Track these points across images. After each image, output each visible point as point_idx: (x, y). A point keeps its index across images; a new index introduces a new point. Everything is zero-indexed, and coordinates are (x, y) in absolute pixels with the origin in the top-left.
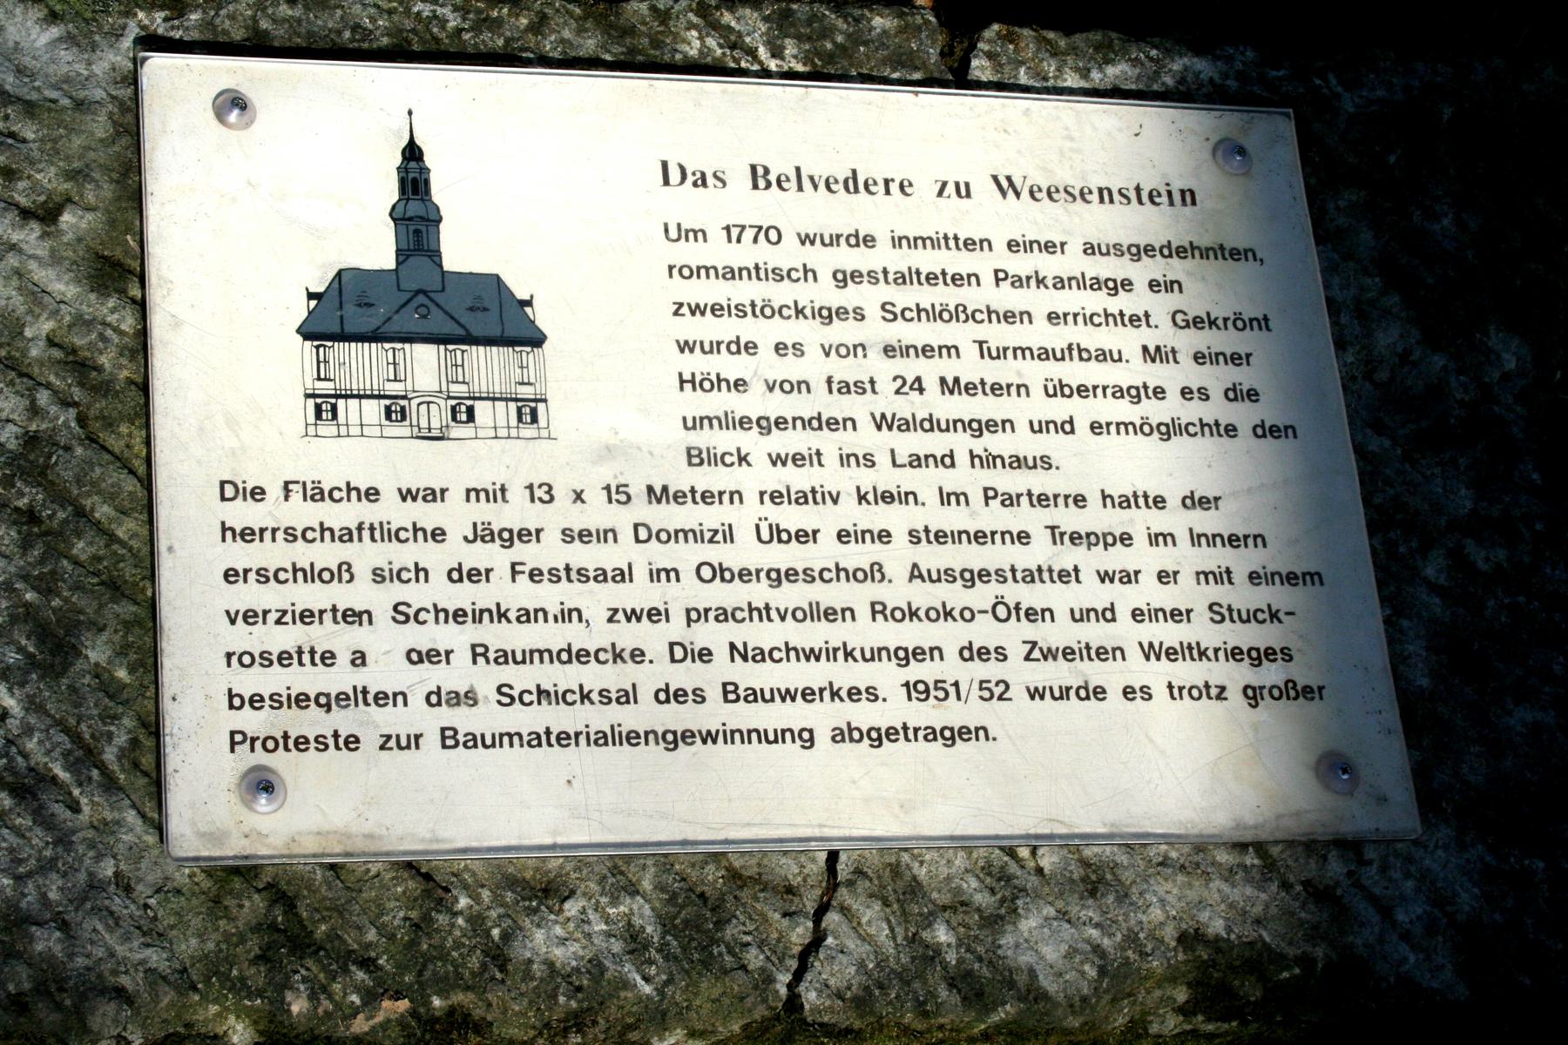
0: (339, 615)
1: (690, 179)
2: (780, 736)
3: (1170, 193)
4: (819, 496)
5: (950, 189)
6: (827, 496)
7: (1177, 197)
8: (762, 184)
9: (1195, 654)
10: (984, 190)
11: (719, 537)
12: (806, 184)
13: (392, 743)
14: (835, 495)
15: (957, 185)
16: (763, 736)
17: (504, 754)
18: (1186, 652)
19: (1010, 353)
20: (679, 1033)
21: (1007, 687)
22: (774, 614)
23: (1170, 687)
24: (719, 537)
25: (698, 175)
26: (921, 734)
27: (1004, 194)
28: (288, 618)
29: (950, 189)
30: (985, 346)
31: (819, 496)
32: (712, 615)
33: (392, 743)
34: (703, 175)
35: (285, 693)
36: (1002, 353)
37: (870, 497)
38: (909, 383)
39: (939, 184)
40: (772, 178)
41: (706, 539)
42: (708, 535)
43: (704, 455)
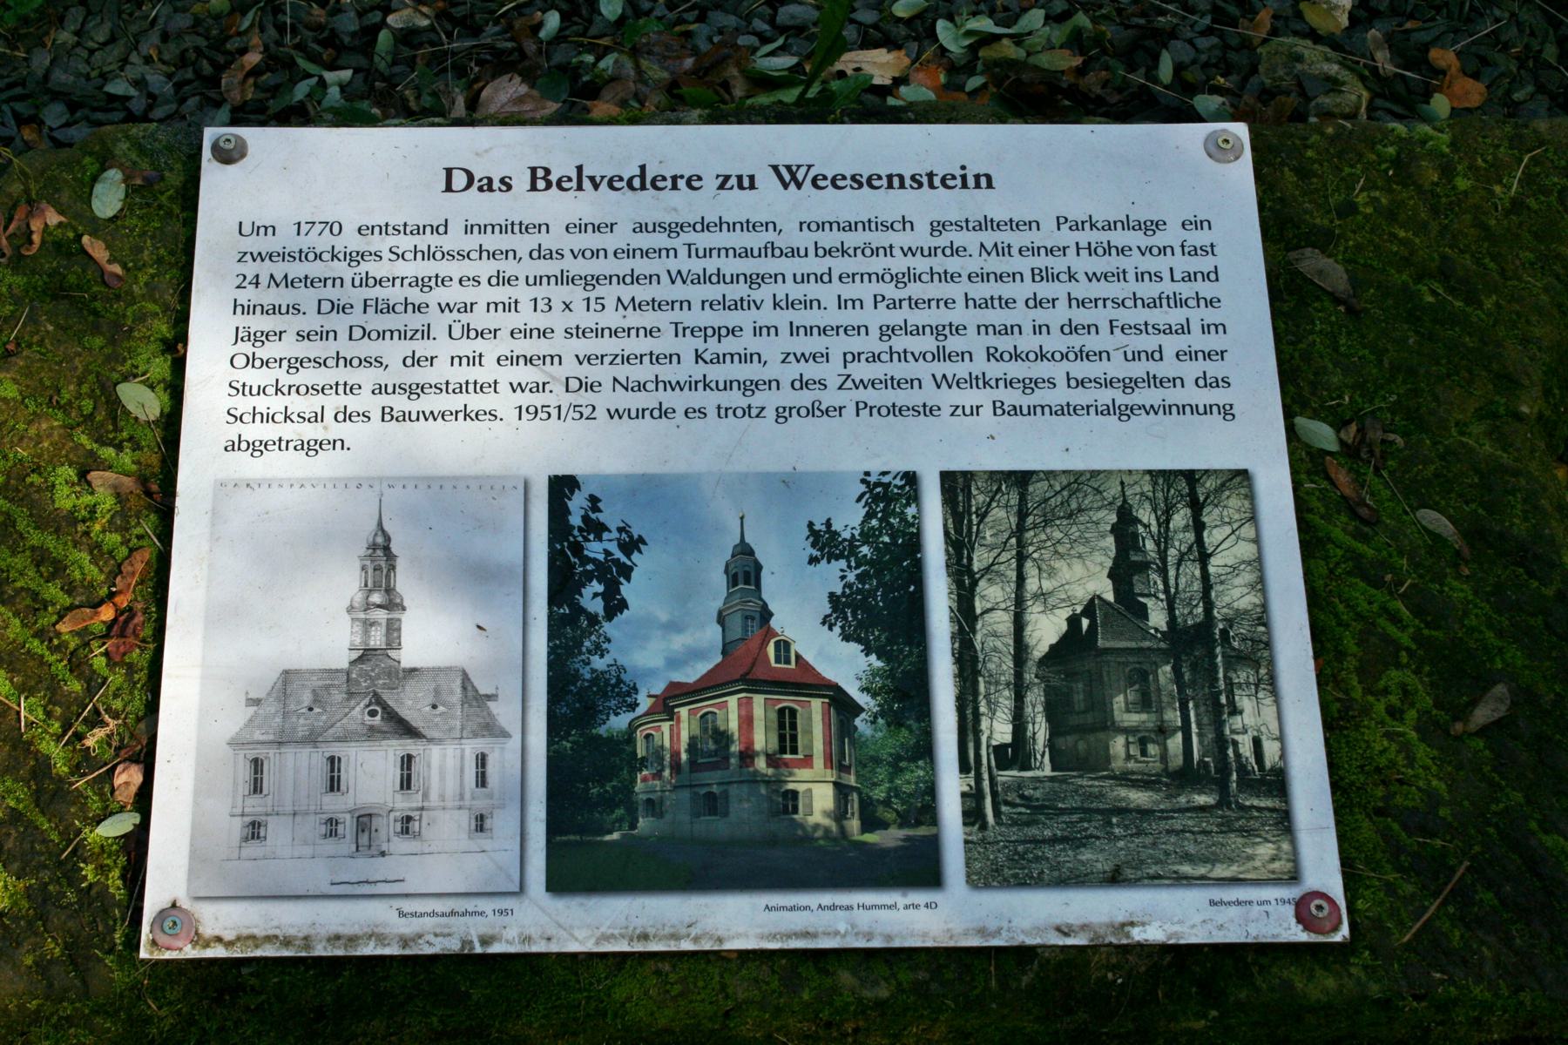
0: (654, 358)
1: (476, 184)
2: (1208, 410)
3: (964, 177)
4: (745, 304)
5: (733, 181)
6: (752, 304)
7: (971, 182)
8: (541, 184)
9: (981, 383)
10: (767, 180)
11: (419, 335)
12: (587, 184)
13: (959, 411)
14: (758, 303)
15: (740, 178)
16: (1194, 409)
17: (1038, 420)
18: (974, 382)
19: (715, 253)
20: (829, 611)
21: (594, 408)
22: (909, 357)
23: (719, 407)
24: (419, 335)
25: (485, 181)
26: (291, 445)
27: (786, 186)
28: (619, 360)
29: (733, 181)
30: (693, 248)
31: (745, 304)
32: (863, 357)
33: (959, 411)
34: (490, 180)
35: (1103, 377)
36: (708, 253)
37: (783, 304)
38: (248, 280)
39: (721, 179)
40: (554, 178)
41: (408, 337)
42: (409, 334)
43: (1044, 274)
